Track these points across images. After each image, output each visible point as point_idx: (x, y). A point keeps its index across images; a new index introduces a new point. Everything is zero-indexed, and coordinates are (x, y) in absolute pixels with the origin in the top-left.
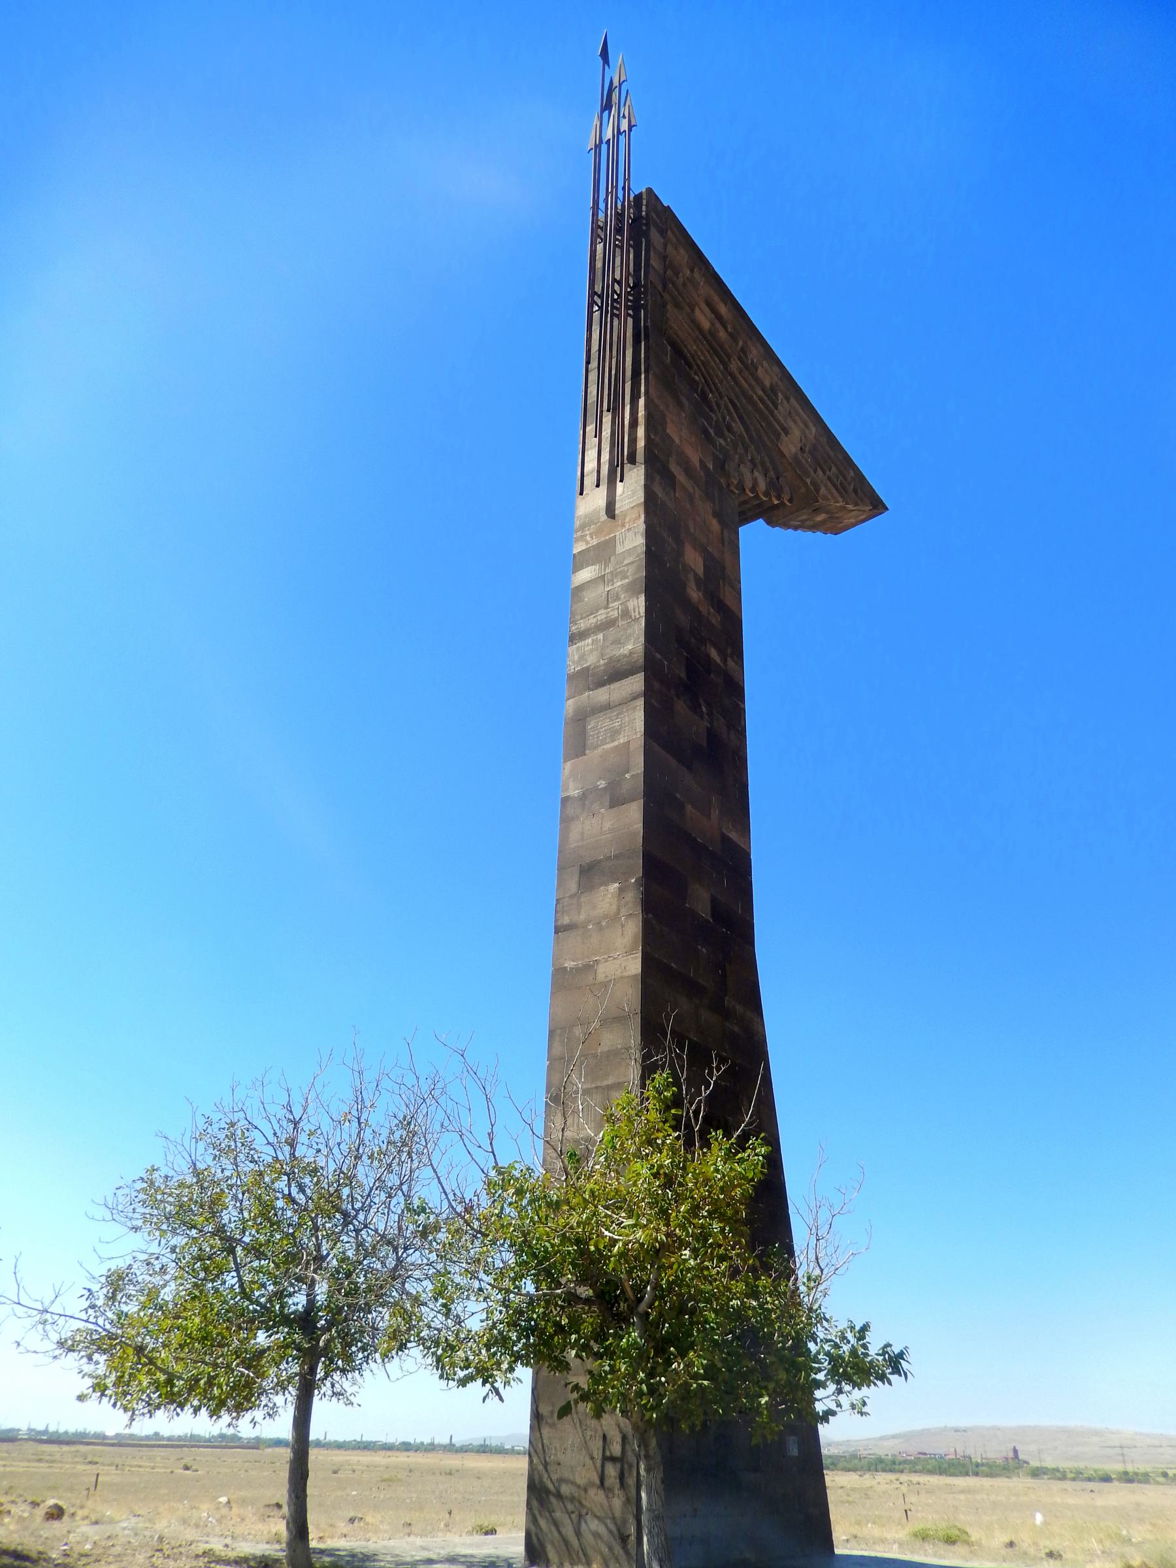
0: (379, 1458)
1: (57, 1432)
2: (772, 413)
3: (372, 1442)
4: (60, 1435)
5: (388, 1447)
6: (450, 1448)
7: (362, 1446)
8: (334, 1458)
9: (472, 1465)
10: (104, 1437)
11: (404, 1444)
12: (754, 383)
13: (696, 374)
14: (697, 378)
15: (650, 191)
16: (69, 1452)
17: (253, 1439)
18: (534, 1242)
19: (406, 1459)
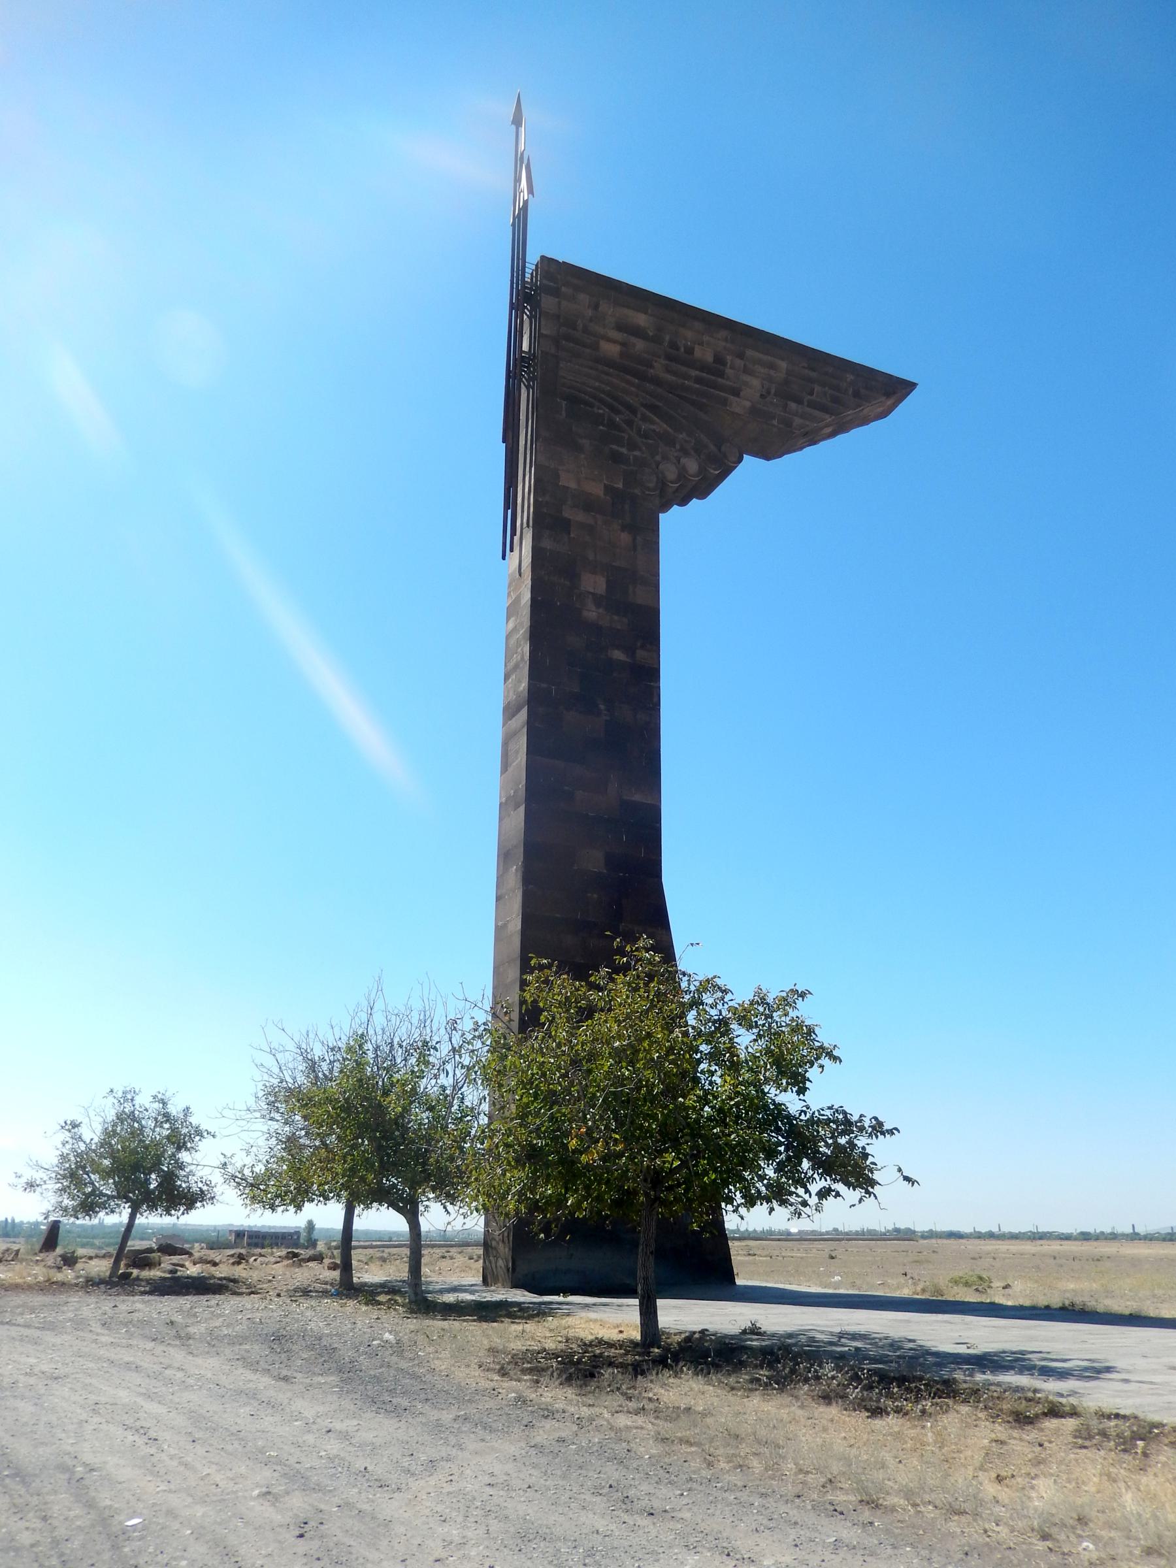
0: (1055, 1247)
1: (747, 1230)
2: (715, 386)
3: (1048, 1233)
4: (749, 1233)
5: (1067, 1237)
6: (1134, 1237)
7: (1037, 1236)
8: (982, 1247)
9: (1127, 1252)
10: (789, 1234)
11: (1082, 1233)
12: (684, 369)
13: (598, 408)
14: (601, 411)
15: (543, 257)
16: (738, 1247)
17: (927, 1232)
18: (119, 1129)
19: (1059, 1247)
